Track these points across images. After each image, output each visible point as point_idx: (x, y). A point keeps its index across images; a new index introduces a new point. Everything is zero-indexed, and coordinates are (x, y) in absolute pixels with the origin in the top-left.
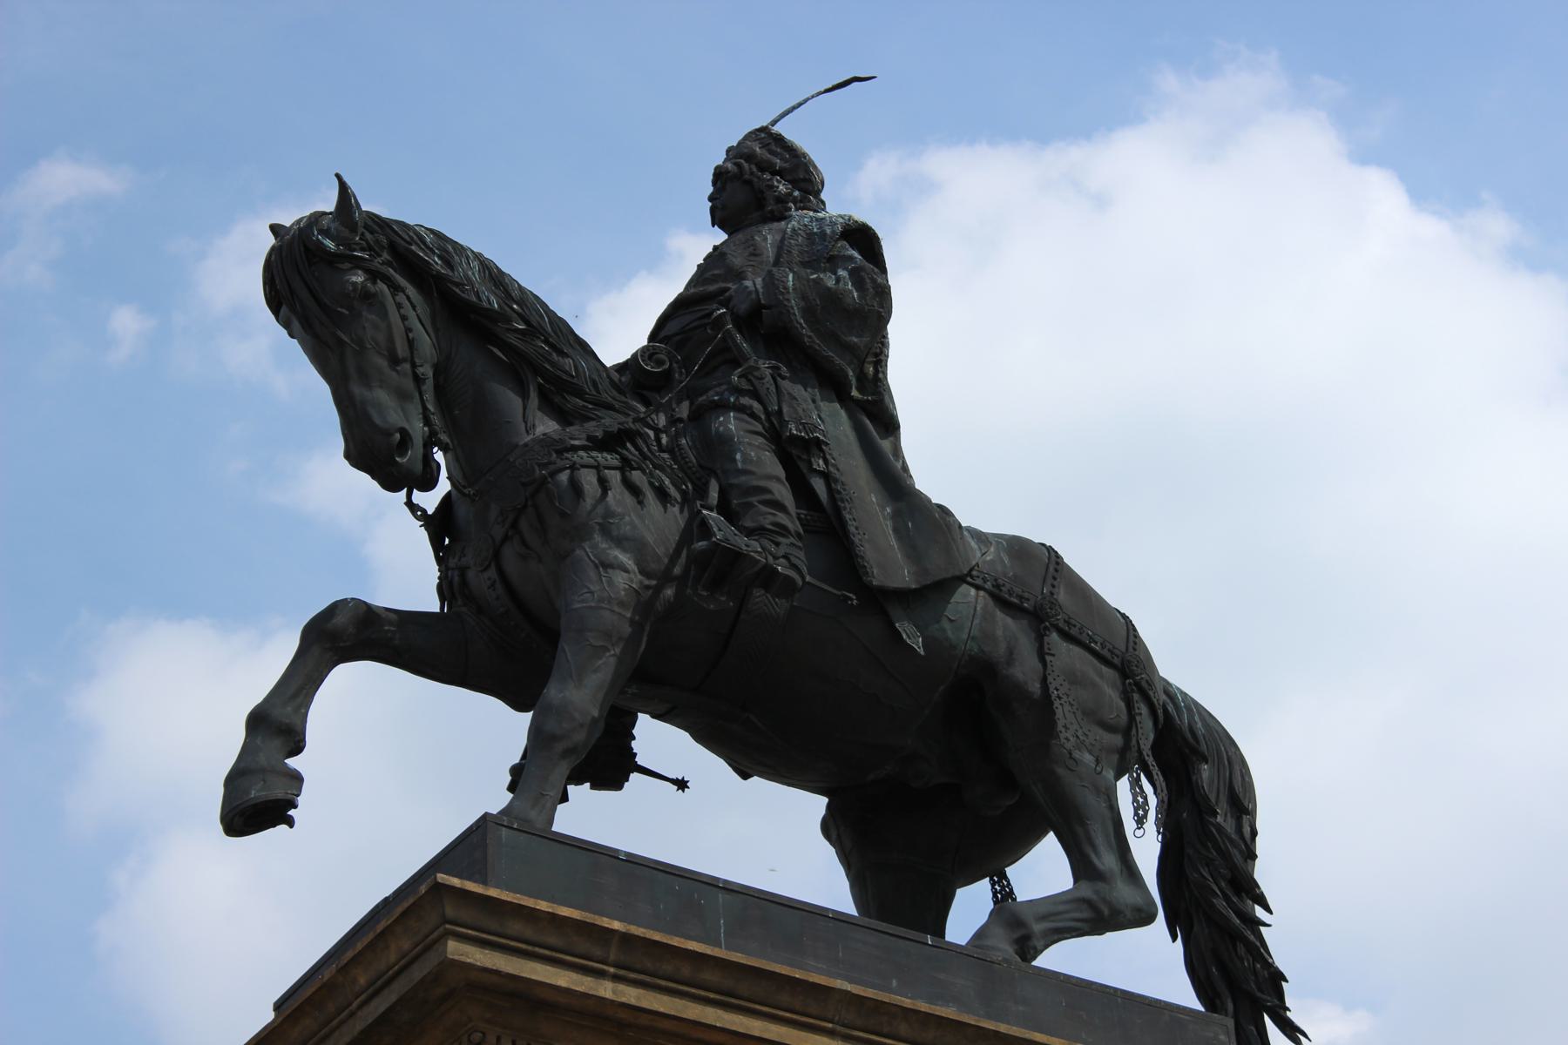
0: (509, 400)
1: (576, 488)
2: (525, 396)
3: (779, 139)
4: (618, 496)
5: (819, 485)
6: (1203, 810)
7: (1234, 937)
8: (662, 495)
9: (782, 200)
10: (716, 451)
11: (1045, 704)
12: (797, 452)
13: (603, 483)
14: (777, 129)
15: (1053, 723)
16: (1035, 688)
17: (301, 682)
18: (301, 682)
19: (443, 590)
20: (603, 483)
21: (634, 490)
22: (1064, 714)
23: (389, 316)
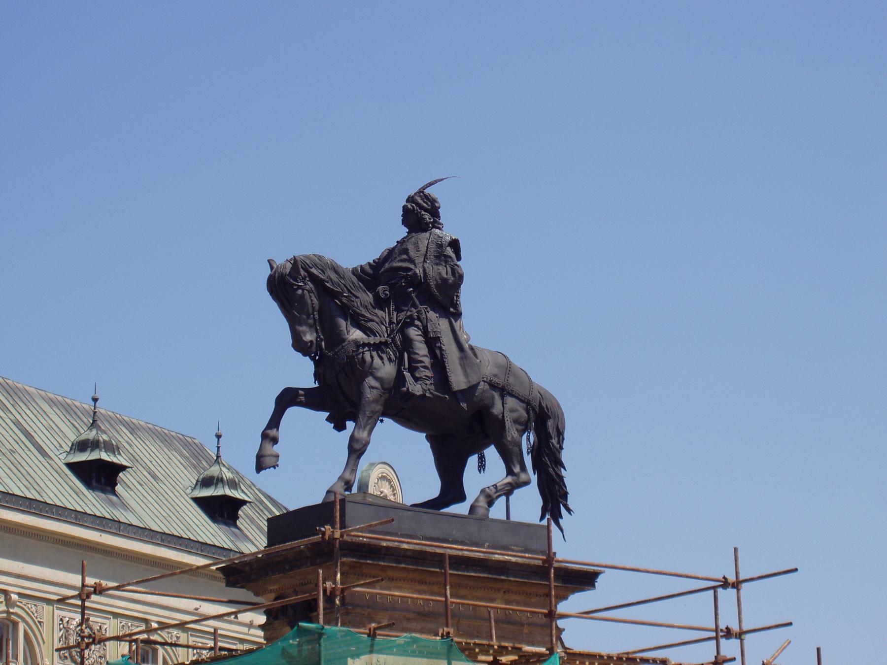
0: (342, 323)
1: (364, 360)
2: (346, 320)
3: (427, 198)
4: (377, 361)
5: (438, 352)
6: (548, 437)
7: (555, 482)
8: (390, 360)
9: (427, 224)
10: (407, 343)
11: (503, 422)
12: (432, 342)
13: (372, 357)
14: (427, 191)
15: (505, 427)
16: (500, 416)
17: (275, 421)
18: (275, 421)
19: (317, 376)
20: (372, 357)
21: (381, 358)
22: (508, 424)
23: (301, 292)
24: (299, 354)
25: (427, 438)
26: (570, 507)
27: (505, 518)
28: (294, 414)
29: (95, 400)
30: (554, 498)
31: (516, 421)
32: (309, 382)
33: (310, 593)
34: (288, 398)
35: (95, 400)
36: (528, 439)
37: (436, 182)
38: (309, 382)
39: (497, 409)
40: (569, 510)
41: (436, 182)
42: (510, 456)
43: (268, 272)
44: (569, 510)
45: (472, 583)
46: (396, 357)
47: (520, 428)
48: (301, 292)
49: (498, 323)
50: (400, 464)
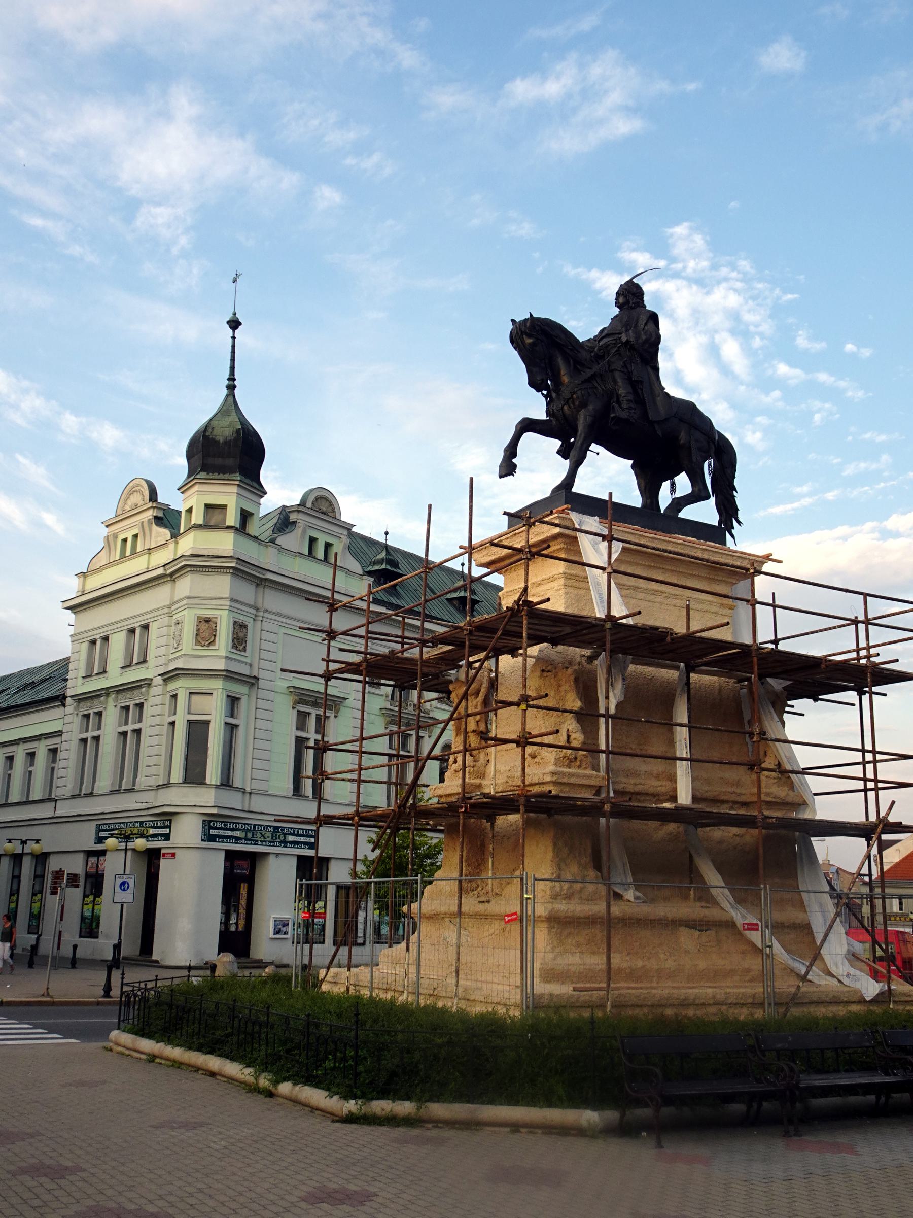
14: (635, 280)
19: (548, 413)
22: (694, 450)
23: (540, 344)
24: (617, 289)
25: (633, 467)
26: (740, 519)
27: (423, 556)
28: (530, 439)
29: (387, 533)
32: (543, 416)
34: (527, 425)
35: (387, 533)
36: (709, 465)
37: (232, 378)
38: (543, 416)
39: (683, 437)
40: (739, 523)
41: (232, 378)
42: (696, 478)
44: (739, 523)
48: (540, 344)
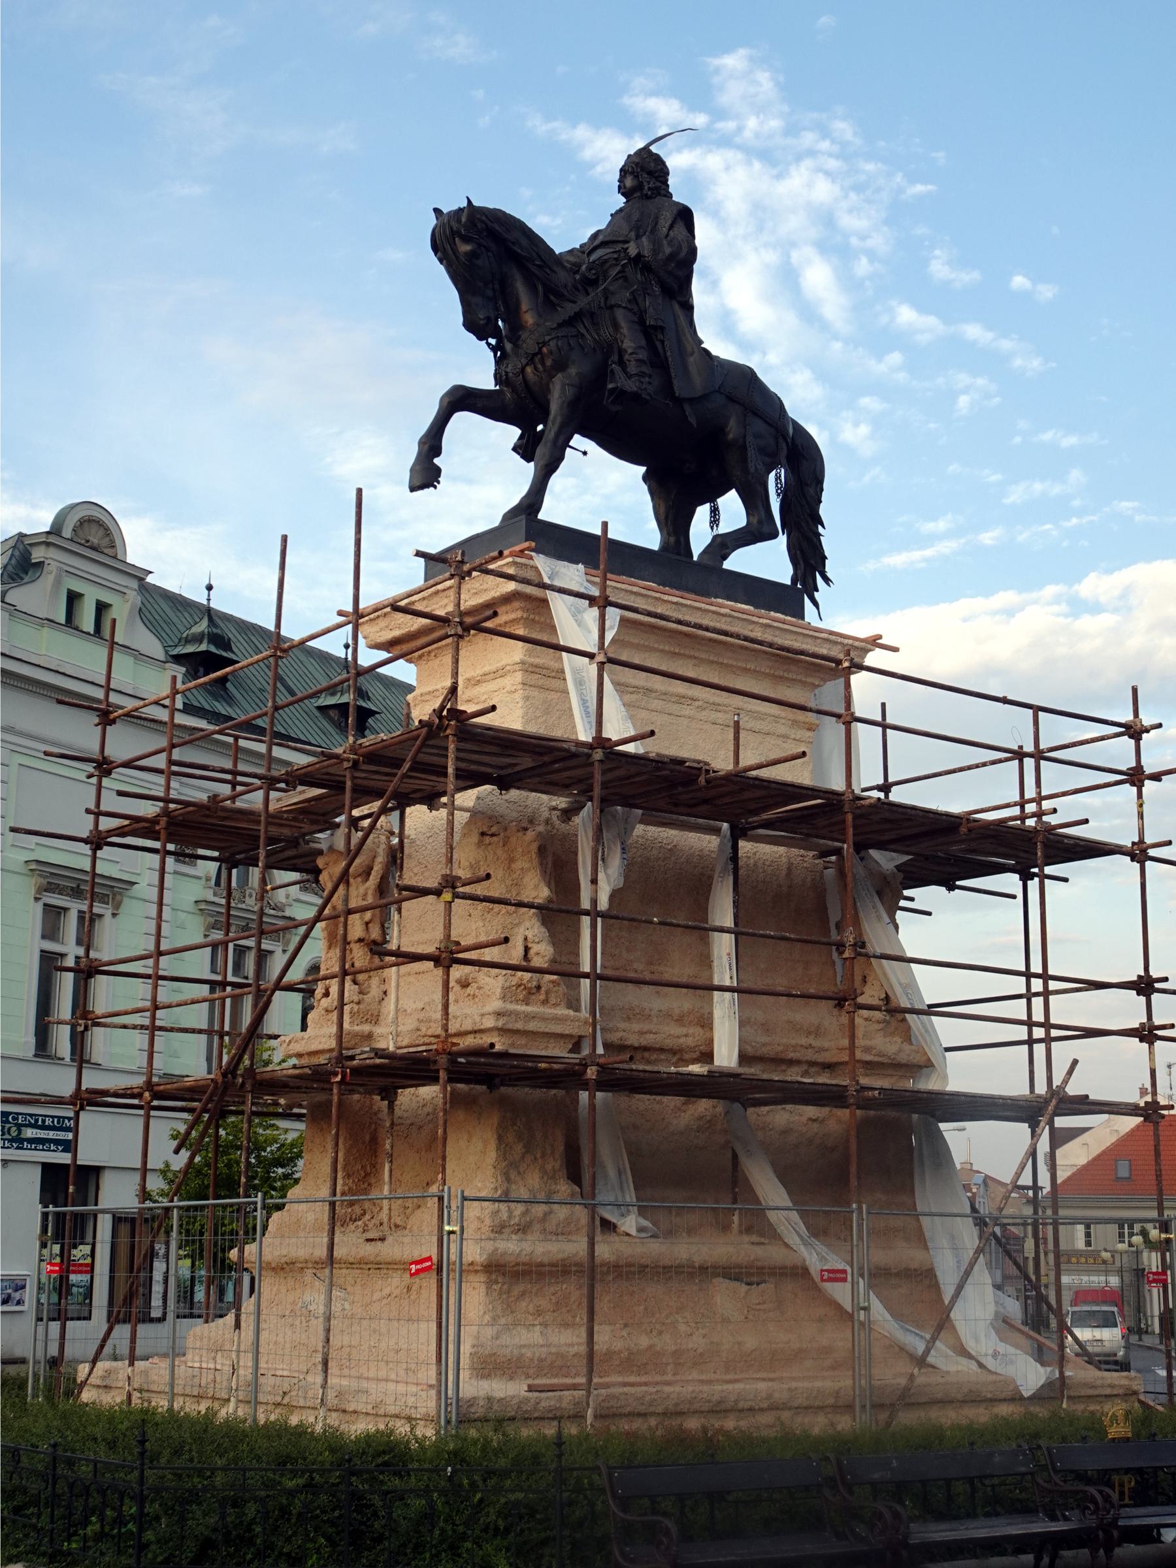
14: (653, 149)
23: (484, 254)
24: (472, 337)
26: (829, 575)
28: (464, 422)
30: (809, 559)
31: (762, 450)
33: (85, 1538)
34: (461, 399)
36: (778, 478)
39: (733, 429)
40: (827, 580)
42: (754, 500)
43: (433, 221)
44: (827, 580)
45: (793, 1075)
46: (594, 262)
47: (768, 460)
48: (484, 254)
49: (736, 311)
50: (602, 490)
